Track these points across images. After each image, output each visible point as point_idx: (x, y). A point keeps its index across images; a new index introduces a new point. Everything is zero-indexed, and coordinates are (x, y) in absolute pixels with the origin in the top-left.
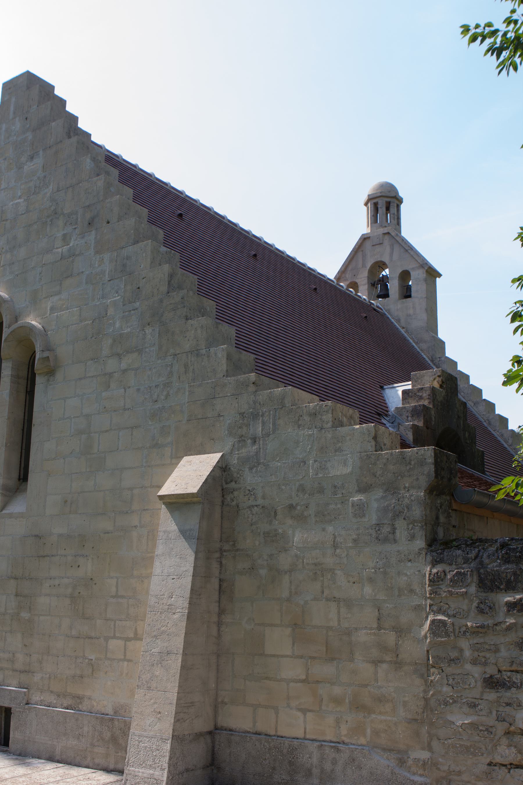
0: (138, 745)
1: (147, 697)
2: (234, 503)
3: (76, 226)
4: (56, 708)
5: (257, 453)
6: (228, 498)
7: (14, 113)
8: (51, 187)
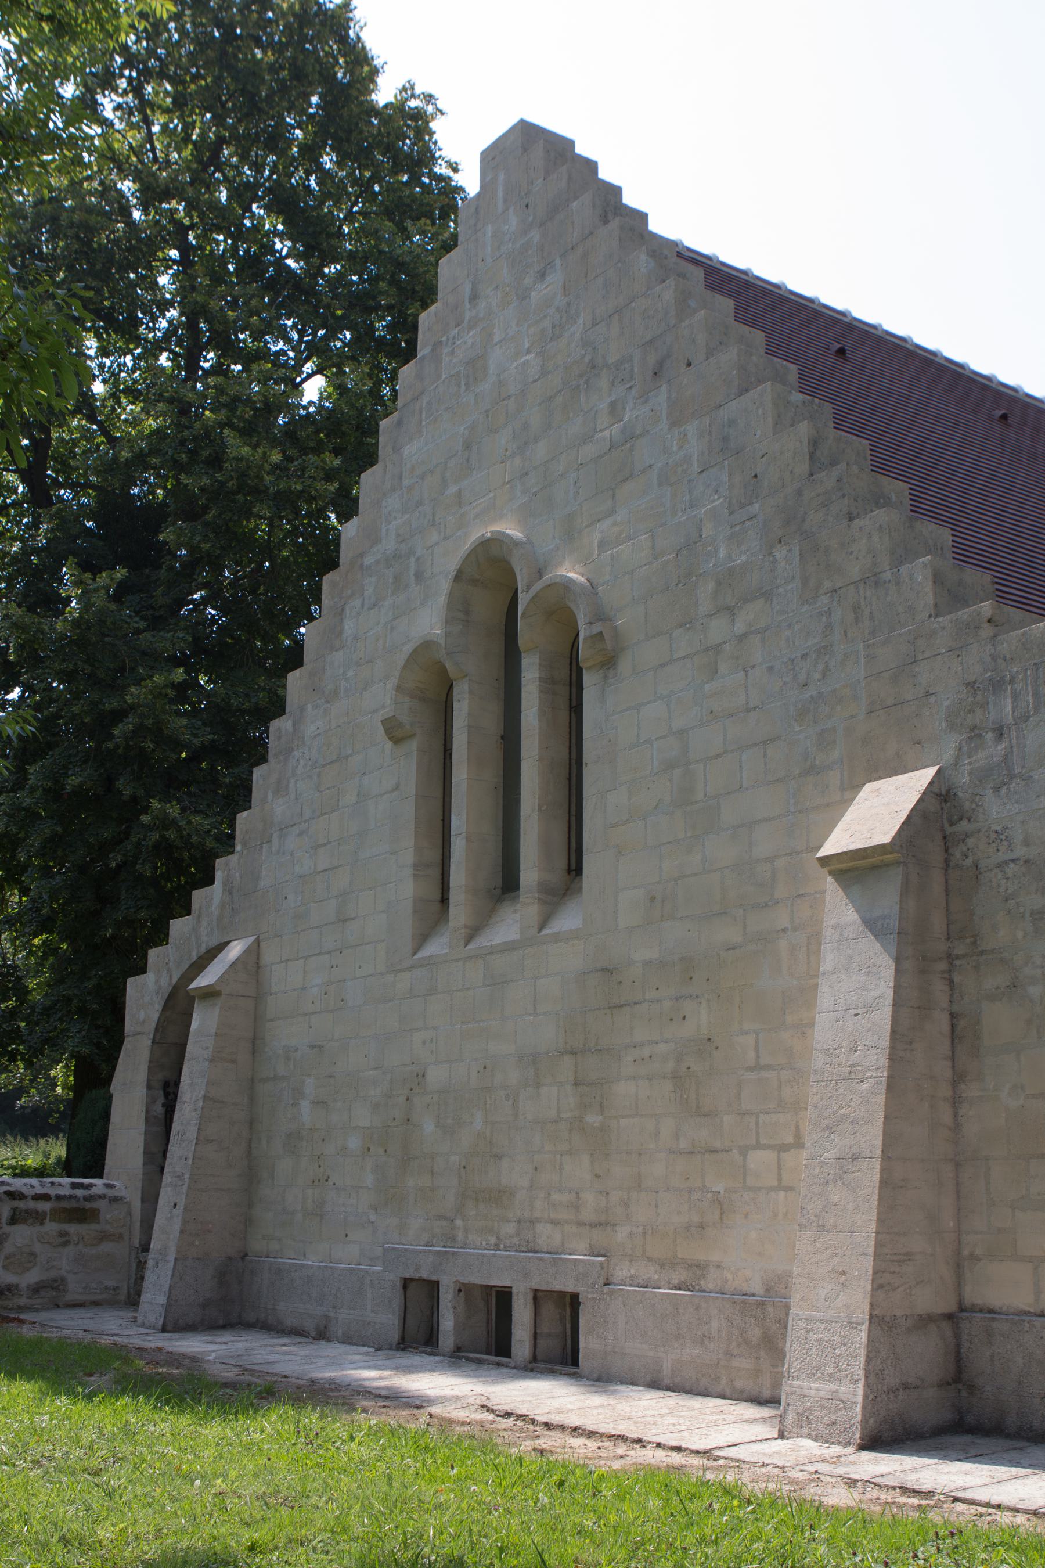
0: (806, 1338)
1: (819, 1245)
2: (969, 862)
3: (633, 383)
4: (659, 1288)
5: (1007, 757)
6: (957, 853)
7: (505, 201)
8: (581, 321)
